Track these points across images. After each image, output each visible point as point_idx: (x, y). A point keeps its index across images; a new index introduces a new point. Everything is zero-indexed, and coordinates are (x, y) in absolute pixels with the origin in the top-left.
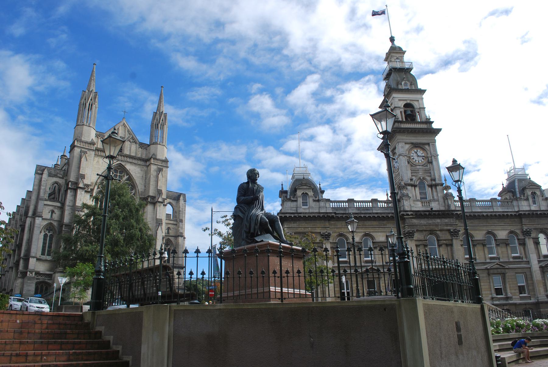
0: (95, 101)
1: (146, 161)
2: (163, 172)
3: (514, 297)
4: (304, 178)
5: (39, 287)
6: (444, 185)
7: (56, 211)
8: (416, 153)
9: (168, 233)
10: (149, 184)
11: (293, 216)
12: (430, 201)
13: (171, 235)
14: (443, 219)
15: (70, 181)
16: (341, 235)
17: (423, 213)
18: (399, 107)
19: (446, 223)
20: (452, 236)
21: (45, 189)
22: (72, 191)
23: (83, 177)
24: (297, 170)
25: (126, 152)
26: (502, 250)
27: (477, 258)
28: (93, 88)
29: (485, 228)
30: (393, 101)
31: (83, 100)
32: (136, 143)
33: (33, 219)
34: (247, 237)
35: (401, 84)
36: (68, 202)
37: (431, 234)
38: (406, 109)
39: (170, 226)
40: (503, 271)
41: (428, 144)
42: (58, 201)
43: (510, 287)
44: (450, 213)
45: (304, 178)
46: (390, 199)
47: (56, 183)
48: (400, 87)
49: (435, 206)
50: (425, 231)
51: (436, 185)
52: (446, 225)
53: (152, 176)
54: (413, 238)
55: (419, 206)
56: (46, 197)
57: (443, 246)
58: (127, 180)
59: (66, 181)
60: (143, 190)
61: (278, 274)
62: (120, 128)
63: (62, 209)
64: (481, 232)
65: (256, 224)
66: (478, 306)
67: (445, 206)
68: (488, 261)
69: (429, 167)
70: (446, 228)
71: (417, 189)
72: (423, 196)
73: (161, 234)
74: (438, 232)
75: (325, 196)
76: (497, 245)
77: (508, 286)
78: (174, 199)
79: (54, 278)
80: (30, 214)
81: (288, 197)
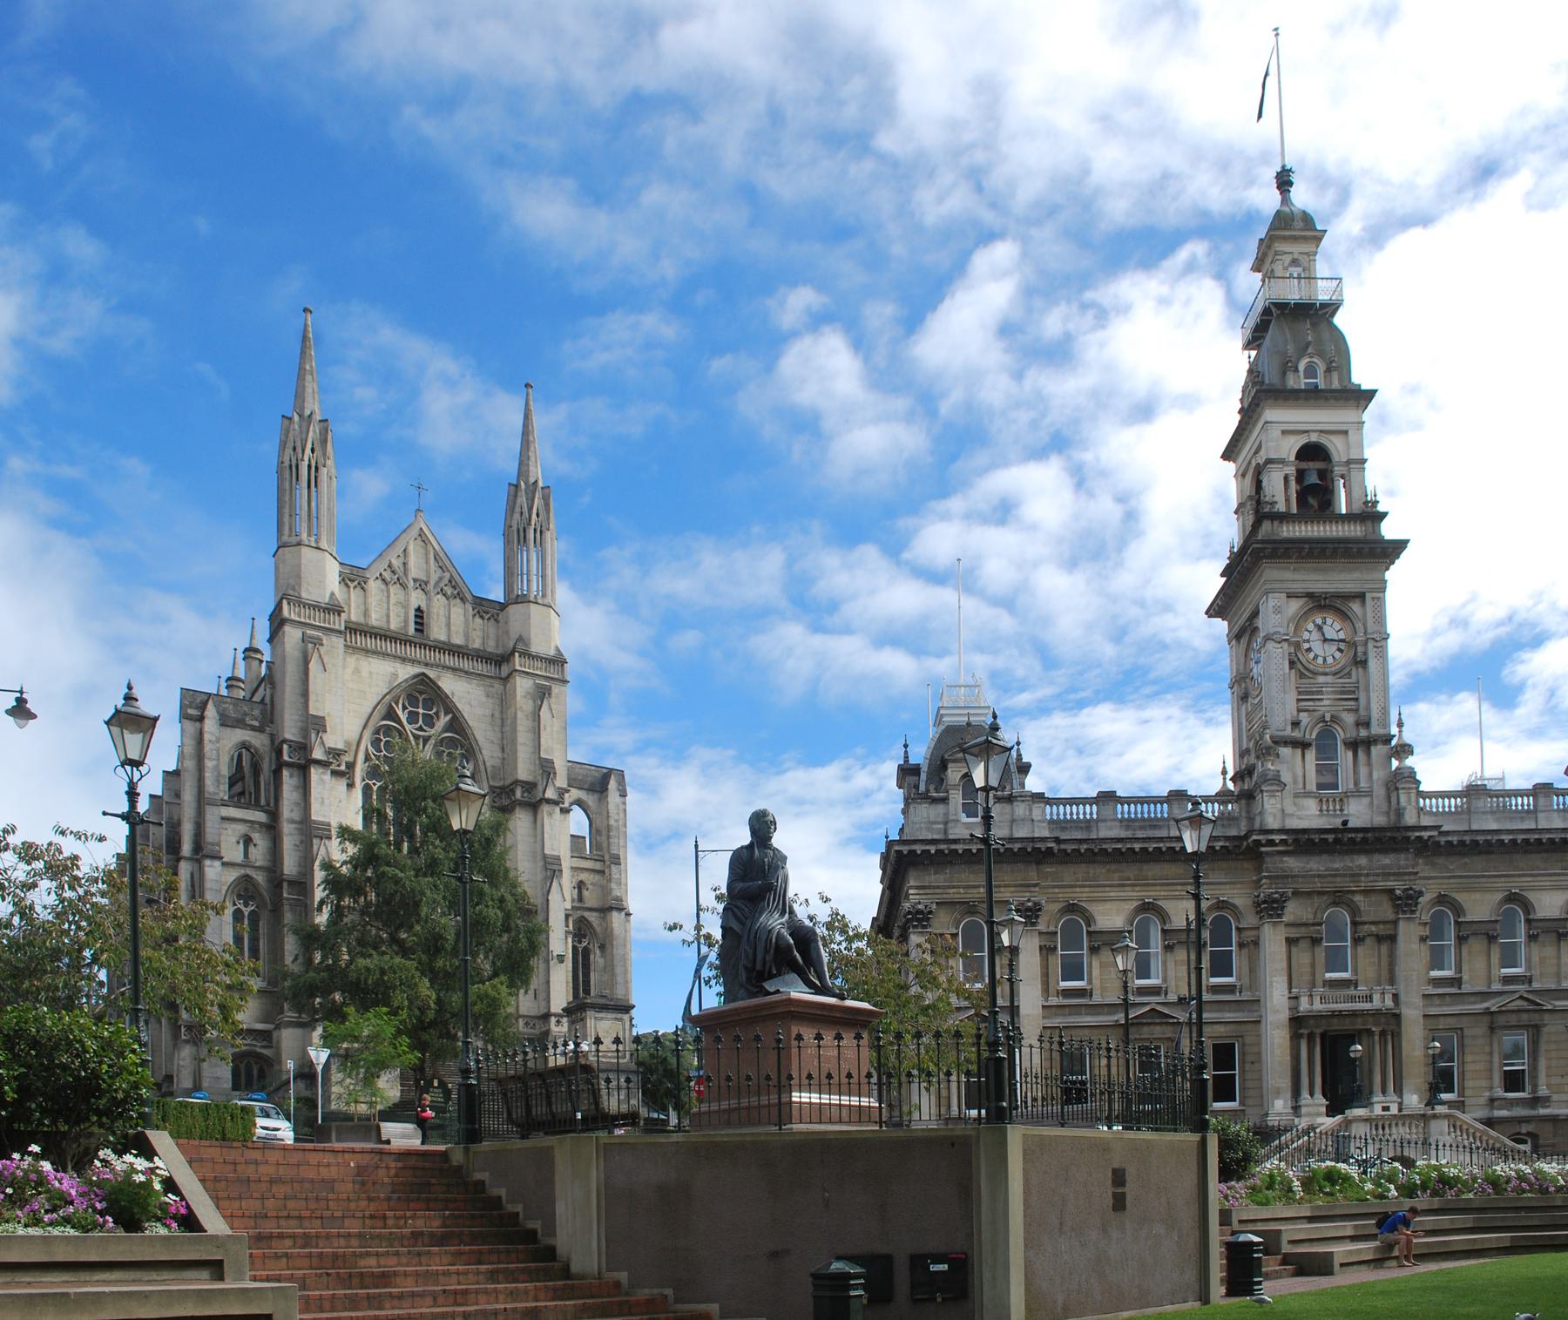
0: (324, 454)
1: (498, 662)
2: (553, 700)
3: (1555, 1097)
4: (969, 724)
5: (242, 1066)
6: (1394, 742)
7: (256, 837)
8: (1320, 628)
9: (580, 899)
10: (514, 741)
11: (933, 849)
12: (1346, 795)
13: (588, 905)
14: (1376, 857)
15: (285, 741)
16: (1072, 908)
17: (1316, 837)
18: (1282, 461)
19: (1384, 867)
20: (1398, 908)
21: (217, 768)
22: (296, 772)
23: (319, 725)
25: (437, 632)
26: (1543, 952)
27: (1465, 977)
28: (312, 405)
29: (1502, 883)
30: (1263, 437)
31: (289, 451)
32: (463, 600)
33: (196, 866)
34: (749, 979)
35: (1296, 370)
36: (288, 810)
37: (1335, 904)
38: (1304, 465)
39: (584, 876)
40: (1536, 1018)
41: (1361, 597)
42: (256, 805)
43: (1548, 1068)
44: (1398, 835)
45: (969, 724)
46: (1231, 786)
47: (245, 746)
48: (1292, 382)
49: (1360, 814)
50: (1320, 893)
51: (1368, 743)
52: (1384, 874)
53: (519, 715)
54: (1280, 916)
55: (1309, 815)
56: (223, 792)
57: (1369, 941)
58: (446, 730)
59: (272, 741)
60: (497, 762)
61: (774, 1082)
62: (411, 548)
63: (272, 828)
64: (1488, 896)
65: (767, 951)
66: (1196, 1137)
67: (1388, 813)
68: (1496, 987)
69: (1354, 679)
70: (1381, 884)
71: (1311, 755)
72: (1328, 779)
73: (560, 903)
74: (1358, 898)
75: (1033, 783)
76: (1532, 938)
77: (1542, 1063)
78: (591, 789)
79: (278, 1042)
80: (186, 848)
81: (922, 788)
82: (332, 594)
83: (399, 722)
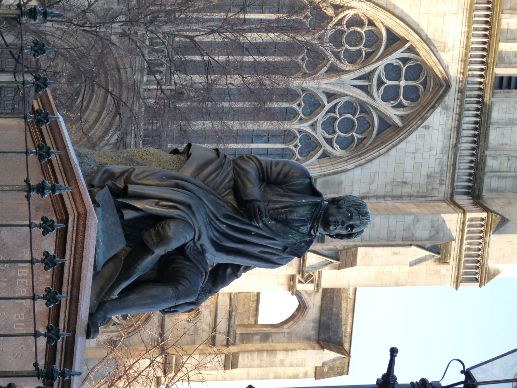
24: (313, 320)
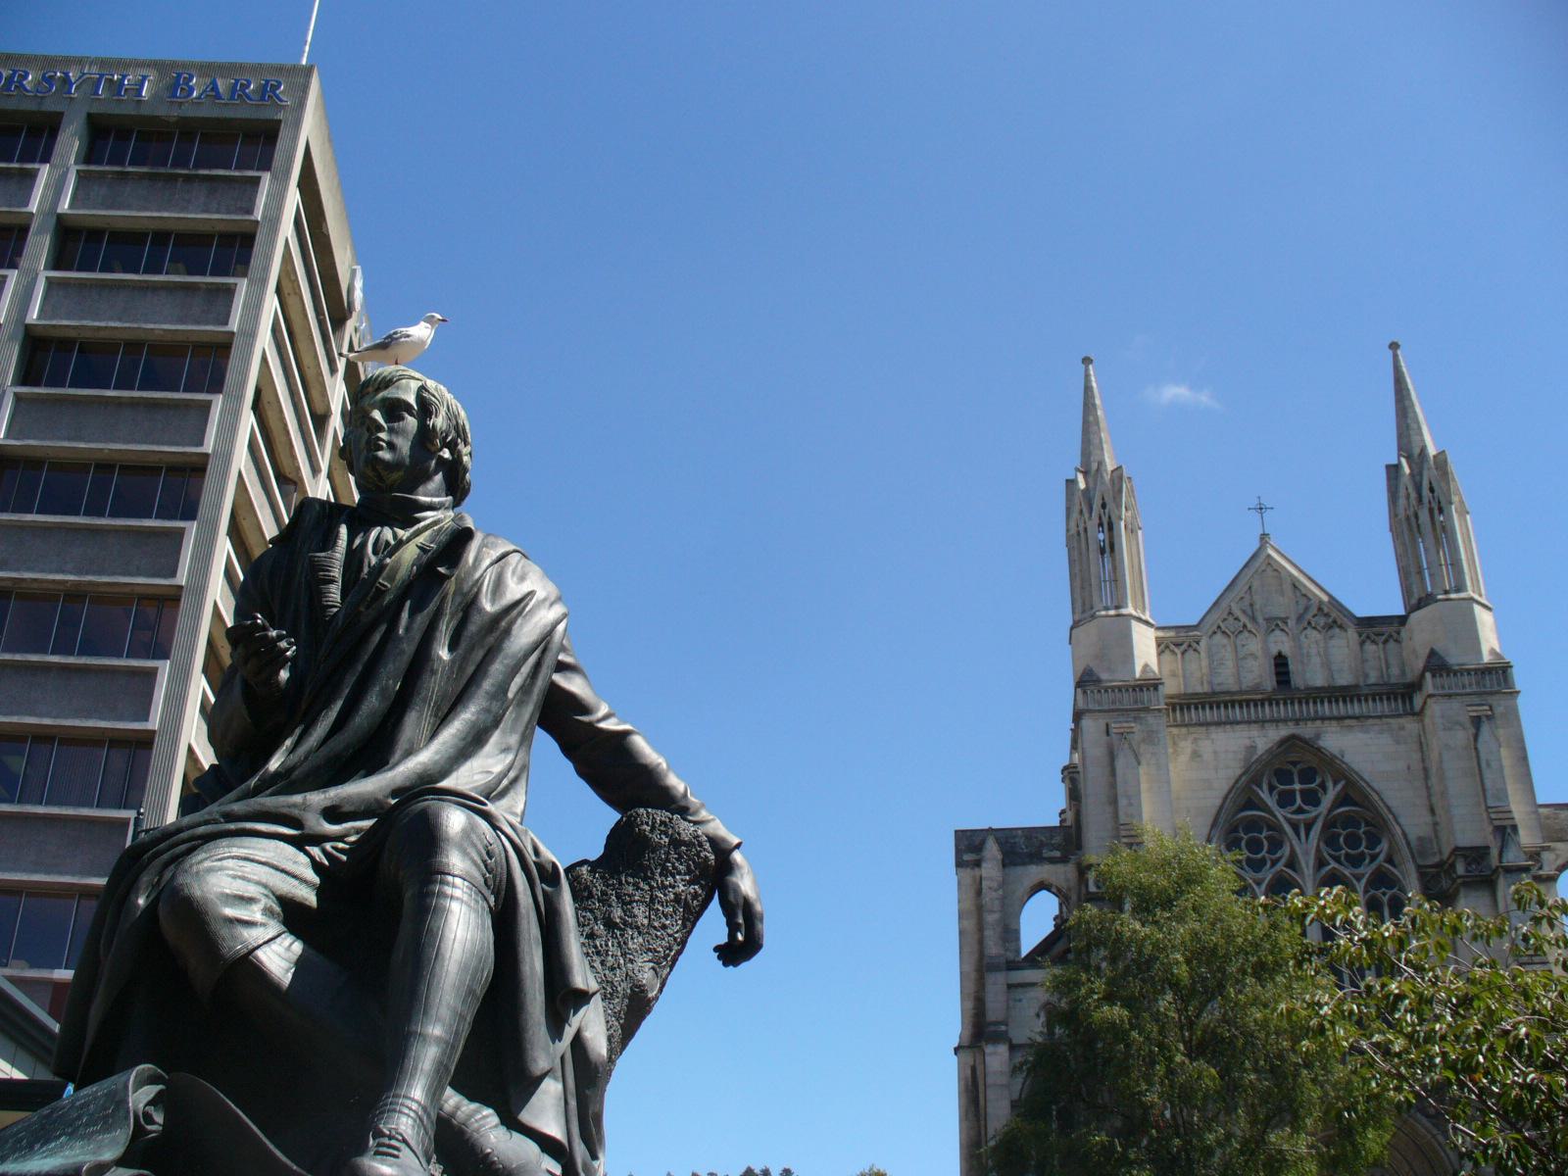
82: (1146, 666)
83: (1266, 809)
